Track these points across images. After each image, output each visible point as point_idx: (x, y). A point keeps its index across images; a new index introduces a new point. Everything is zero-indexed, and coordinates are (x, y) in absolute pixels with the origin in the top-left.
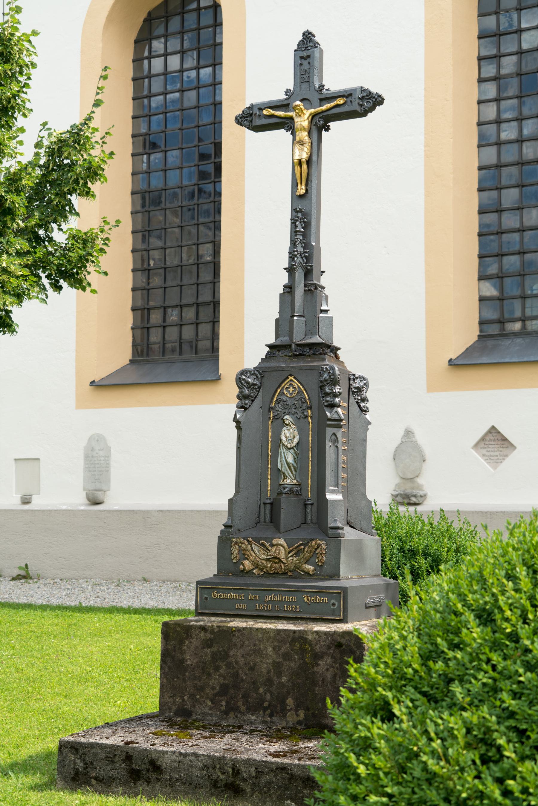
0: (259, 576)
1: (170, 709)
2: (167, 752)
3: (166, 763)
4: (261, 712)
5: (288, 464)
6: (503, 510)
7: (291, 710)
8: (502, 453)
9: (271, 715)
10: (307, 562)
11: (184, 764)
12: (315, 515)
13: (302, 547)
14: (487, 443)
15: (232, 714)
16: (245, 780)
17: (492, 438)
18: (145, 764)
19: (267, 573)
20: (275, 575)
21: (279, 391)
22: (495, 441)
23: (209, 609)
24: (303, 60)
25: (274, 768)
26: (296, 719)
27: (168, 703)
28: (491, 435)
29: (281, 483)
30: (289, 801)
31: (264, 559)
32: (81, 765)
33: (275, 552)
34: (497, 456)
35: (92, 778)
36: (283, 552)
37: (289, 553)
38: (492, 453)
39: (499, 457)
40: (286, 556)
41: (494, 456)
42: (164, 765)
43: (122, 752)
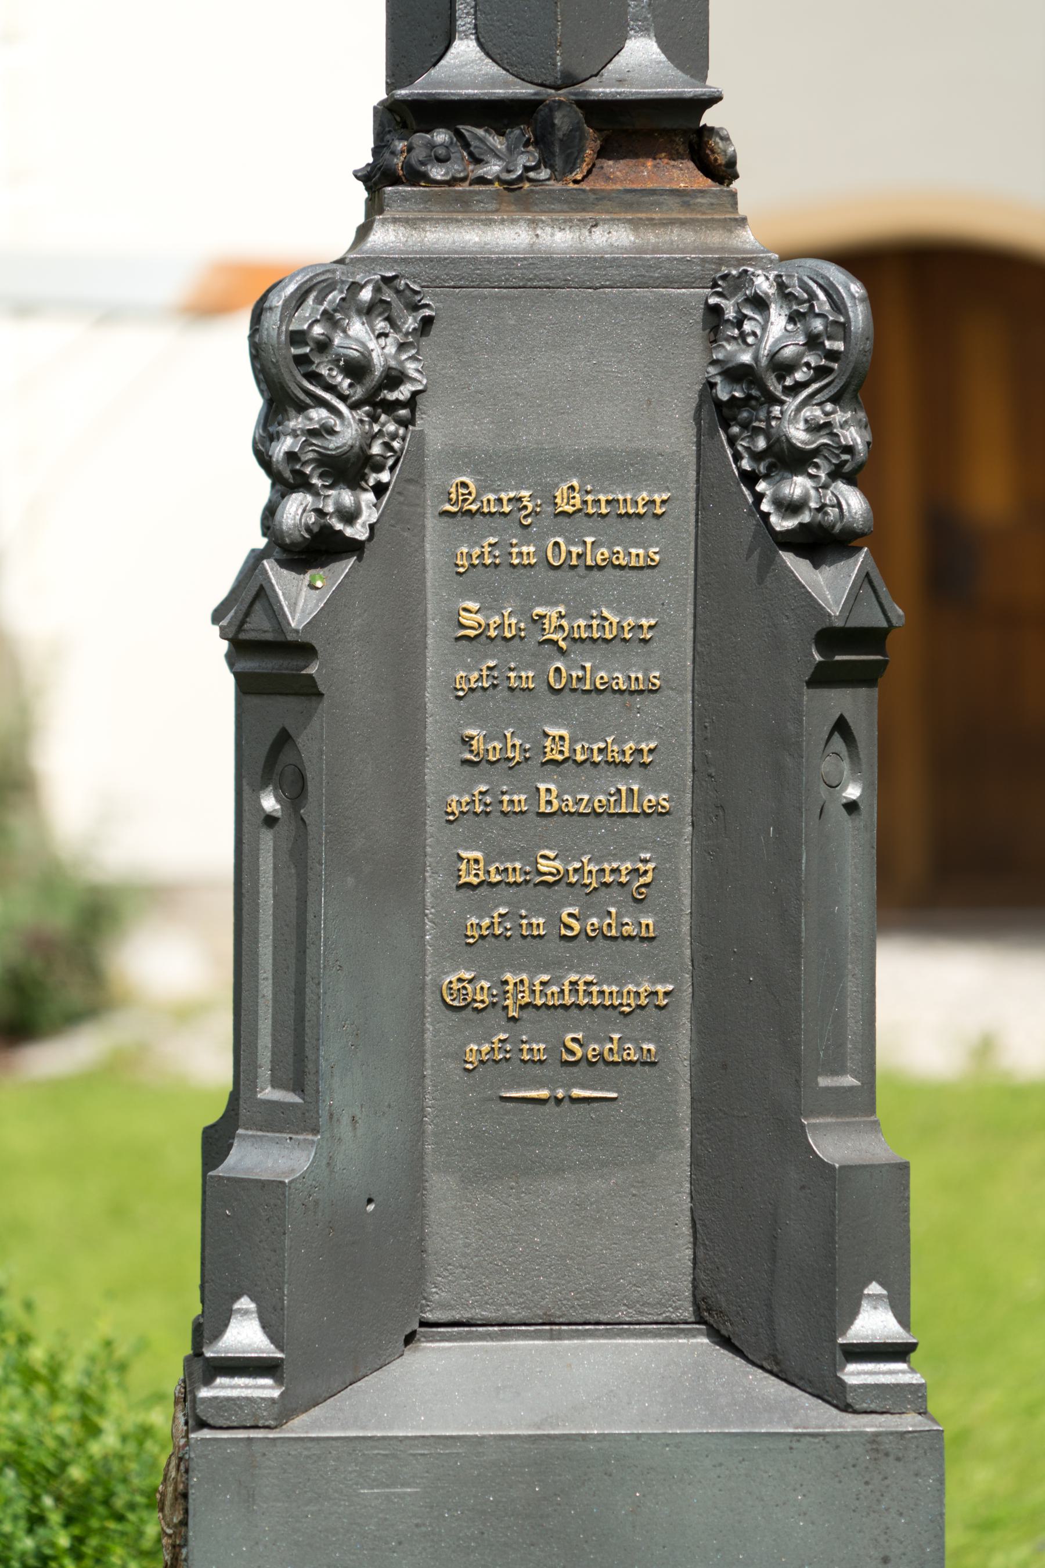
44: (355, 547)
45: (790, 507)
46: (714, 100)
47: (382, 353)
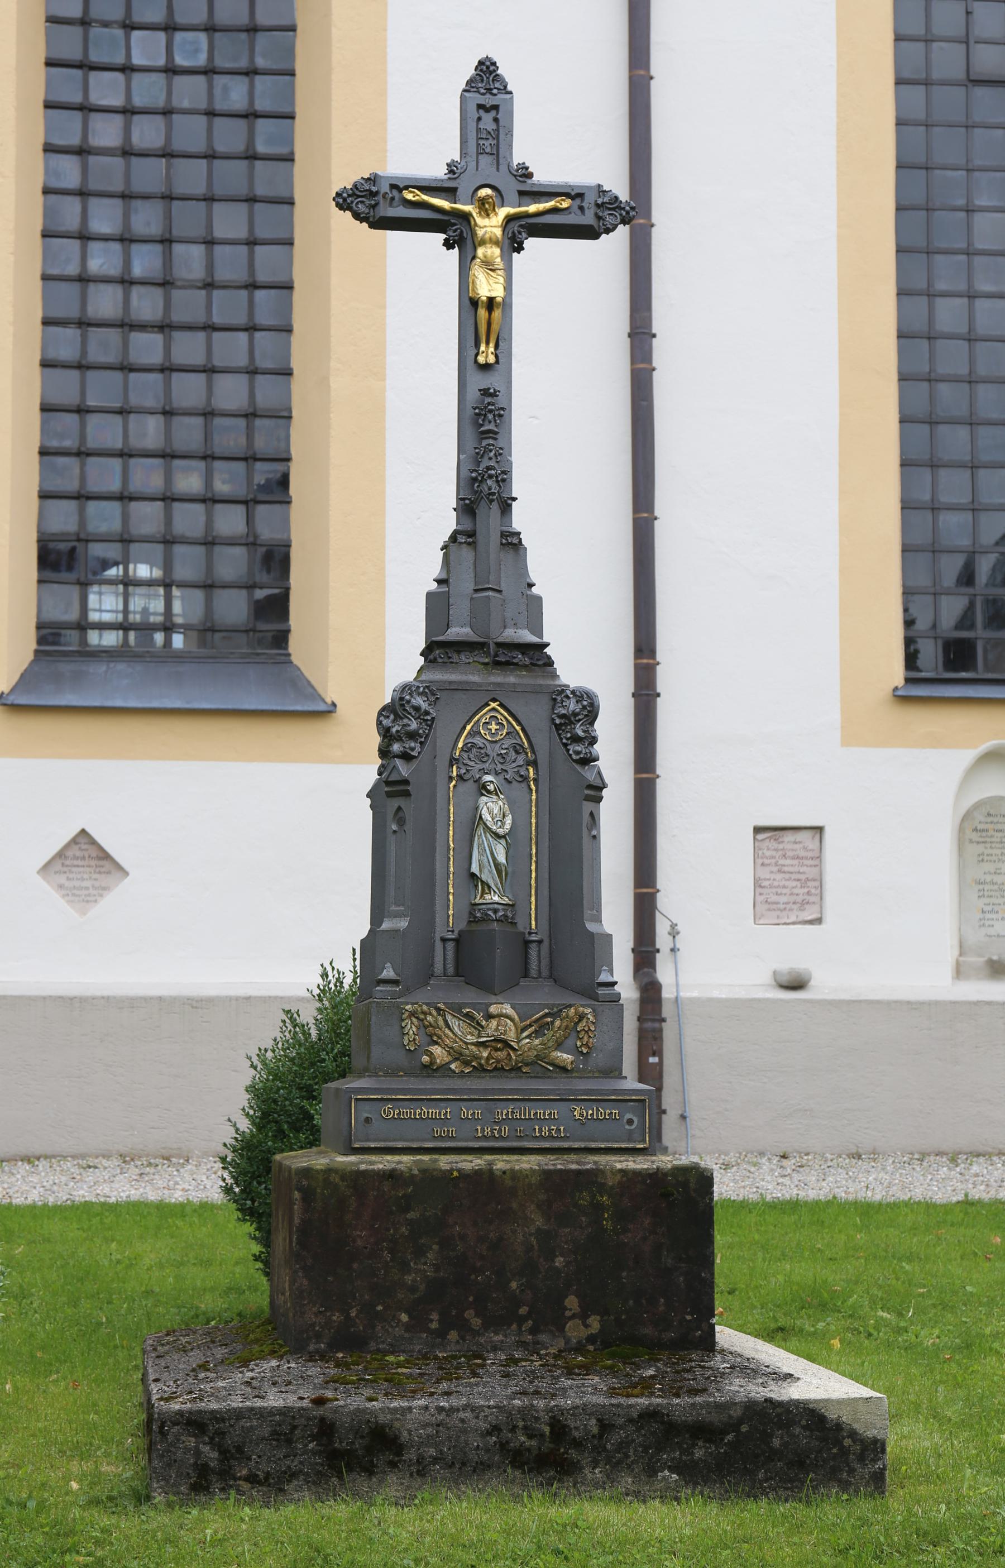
0: (462, 1075)
1: (318, 1337)
2: (410, 1409)
3: (410, 1431)
4: (514, 1326)
5: (497, 865)
6: (105, 993)
7: (573, 1317)
8: (97, 884)
9: (533, 1331)
10: (559, 1046)
11: (448, 1428)
12: (545, 962)
13: (549, 1019)
14: (68, 862)
15: (453, 1335)
16: (577, 1444)
17: (78, 854)
18: (362, 1437)
19: (481, 1070)
20: (494, 1074)
21: (468, 727)
22: (85, 860)
23: (375, 1141)
24: (482, 112)
25: (635, 1415)
26: (583, 1333)
27: (313, 1325)
28: (76, 847)
29: (478, 901)
30: (667, 1473)
31: (472, 1044)
32: (215, 1455)
33: (497, 1030)
34: (87, 888)
35: (240, 1478)
36: (513, 1028)
37: (523, 1030)
38: (77, 883)
39: (91, 891)
40: (517, 1038)
41: (81, 888)
42: (405, 1434)
43: (309, 1419)
44: (414, 757)
45: (578, 753)
46: (547, 645)
47: (424, 706)
